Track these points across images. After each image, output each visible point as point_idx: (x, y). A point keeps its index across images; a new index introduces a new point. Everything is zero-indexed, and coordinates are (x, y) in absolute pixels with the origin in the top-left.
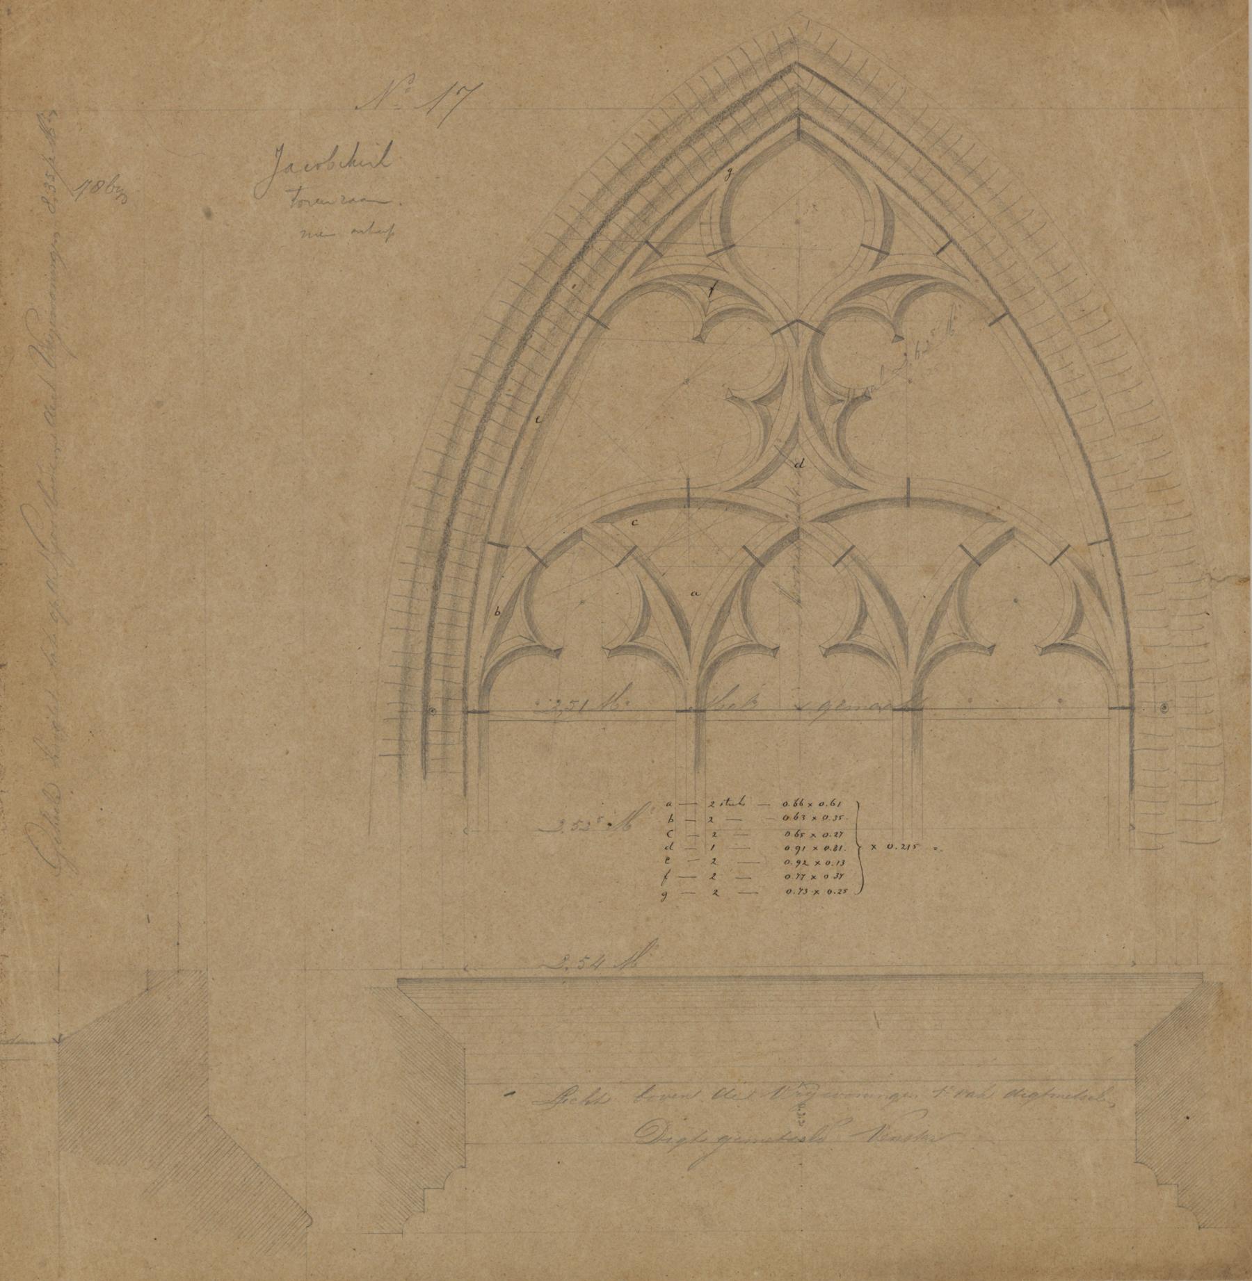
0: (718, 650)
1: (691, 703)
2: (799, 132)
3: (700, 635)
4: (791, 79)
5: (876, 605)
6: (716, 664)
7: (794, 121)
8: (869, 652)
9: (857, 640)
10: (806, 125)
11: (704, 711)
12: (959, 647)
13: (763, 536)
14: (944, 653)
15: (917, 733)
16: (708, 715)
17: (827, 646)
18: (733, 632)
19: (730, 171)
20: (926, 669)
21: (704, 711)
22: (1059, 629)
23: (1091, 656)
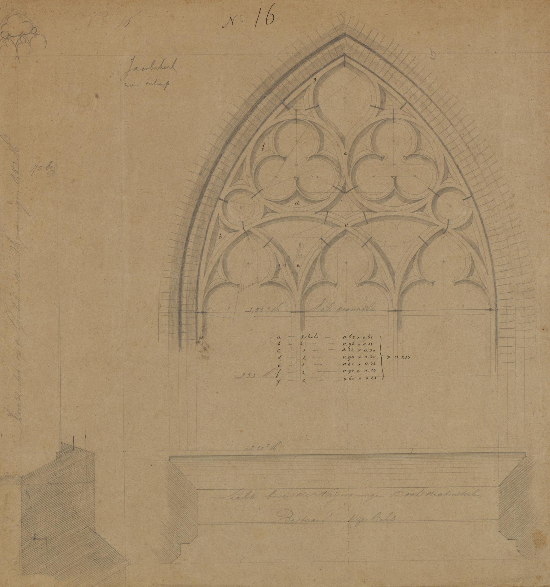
0: (310, 284)
1: (396, 307)
2: (344, 64)
3: (302, 278)
4: (342, 41)
5: (381, 263)
6: (311, 289)
7: (343, 57)
8: (473, 282)
9: (471, 278)
10: (348, 60)
11: (206, 313)
12: (323, 283)
13: (330, 233)
14: (315, 285)
15: (399, 322)
16: (306, 314)
17: (359, 282)
18: (317, 276)
19: (315, 79)
20: (402, 294)
21: (206, 313)
22: (366, 276)
23: (478, 285)
